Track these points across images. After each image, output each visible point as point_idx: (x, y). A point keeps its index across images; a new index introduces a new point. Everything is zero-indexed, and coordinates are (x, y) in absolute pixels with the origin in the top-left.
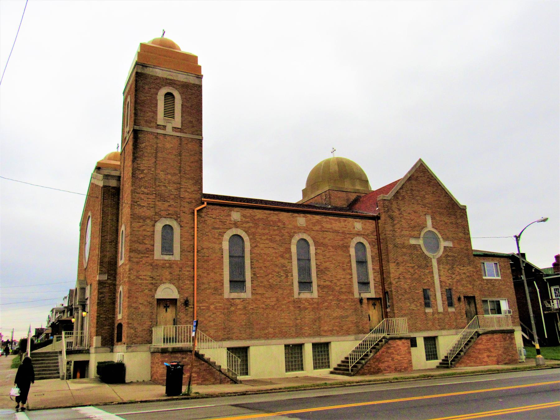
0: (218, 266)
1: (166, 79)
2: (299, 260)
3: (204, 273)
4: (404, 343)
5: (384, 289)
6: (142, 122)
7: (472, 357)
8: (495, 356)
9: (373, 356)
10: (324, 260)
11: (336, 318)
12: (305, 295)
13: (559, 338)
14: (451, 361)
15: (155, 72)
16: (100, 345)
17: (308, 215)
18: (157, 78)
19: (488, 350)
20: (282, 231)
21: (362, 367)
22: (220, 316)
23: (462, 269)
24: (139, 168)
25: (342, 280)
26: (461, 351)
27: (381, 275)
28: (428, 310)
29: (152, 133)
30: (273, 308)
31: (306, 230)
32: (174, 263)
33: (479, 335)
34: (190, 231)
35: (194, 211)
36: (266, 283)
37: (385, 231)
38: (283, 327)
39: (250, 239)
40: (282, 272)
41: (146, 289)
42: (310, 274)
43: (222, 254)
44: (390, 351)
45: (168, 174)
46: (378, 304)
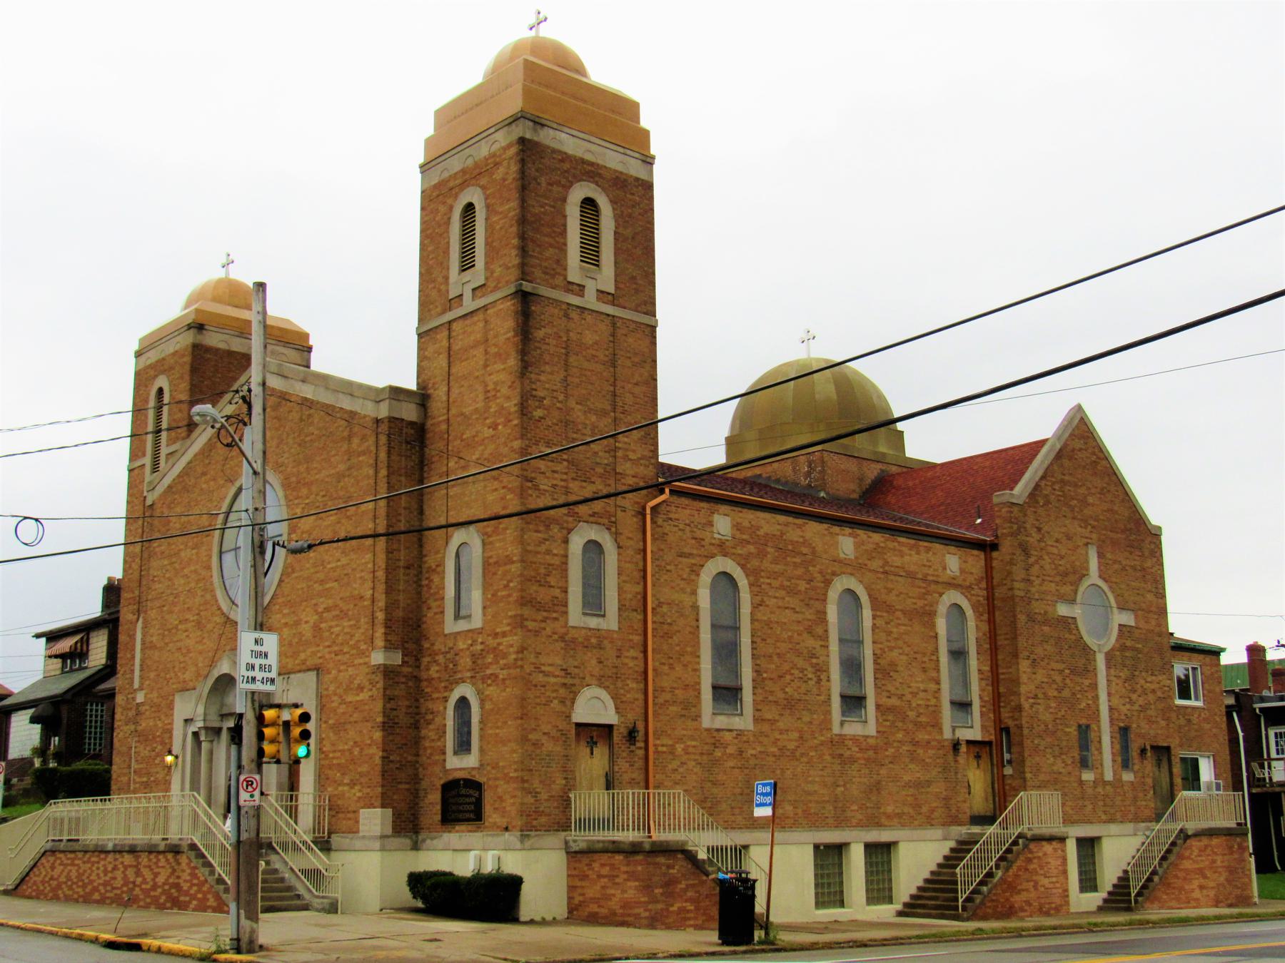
0: (689, 649)
1: (583, 161)
2: (714, 626)
3: (664, 664)
4: (1055, 850)
5: (998, 720)
6: (538, 273)
7: (1174, 888)
8: (1212, 888)
9: (1001, 878)
10: (889, 644)
11: (908, 785)
12: (853, 729)
13: (1276, 853)
14: (963, 902)
15: (560, 141)
16: (389, 831)
17: (859, 532)
18: (565, 157)
19: (1201, 872)
20: (811, 568)
21: (982, 903)
22: (695, 770)
23: (1149, 679)
24: (534, 393)
25: (922, 695)
26: (1154, 873)
27: (993, 685)
28: (1088, 776)
29: (557, 303)
30: (793, 756)
31: (855, 568)
32: (606, 638)
33: (1187, 837)
34: (634, 560)
35: (644, 509)
36: (781, 695)
37: (1013, 581)
38: (811, 801)
39: (751, 585)
40: (810, 669)
41: (554, 698)
42: (861, 682)
43: (697, 620)
44: (1031, 867)
45: (590, 410)
46: (985, 757)
